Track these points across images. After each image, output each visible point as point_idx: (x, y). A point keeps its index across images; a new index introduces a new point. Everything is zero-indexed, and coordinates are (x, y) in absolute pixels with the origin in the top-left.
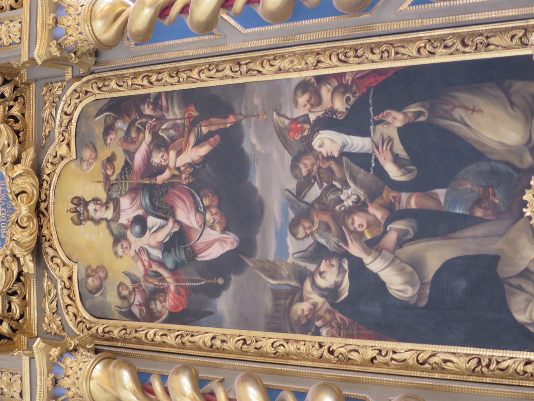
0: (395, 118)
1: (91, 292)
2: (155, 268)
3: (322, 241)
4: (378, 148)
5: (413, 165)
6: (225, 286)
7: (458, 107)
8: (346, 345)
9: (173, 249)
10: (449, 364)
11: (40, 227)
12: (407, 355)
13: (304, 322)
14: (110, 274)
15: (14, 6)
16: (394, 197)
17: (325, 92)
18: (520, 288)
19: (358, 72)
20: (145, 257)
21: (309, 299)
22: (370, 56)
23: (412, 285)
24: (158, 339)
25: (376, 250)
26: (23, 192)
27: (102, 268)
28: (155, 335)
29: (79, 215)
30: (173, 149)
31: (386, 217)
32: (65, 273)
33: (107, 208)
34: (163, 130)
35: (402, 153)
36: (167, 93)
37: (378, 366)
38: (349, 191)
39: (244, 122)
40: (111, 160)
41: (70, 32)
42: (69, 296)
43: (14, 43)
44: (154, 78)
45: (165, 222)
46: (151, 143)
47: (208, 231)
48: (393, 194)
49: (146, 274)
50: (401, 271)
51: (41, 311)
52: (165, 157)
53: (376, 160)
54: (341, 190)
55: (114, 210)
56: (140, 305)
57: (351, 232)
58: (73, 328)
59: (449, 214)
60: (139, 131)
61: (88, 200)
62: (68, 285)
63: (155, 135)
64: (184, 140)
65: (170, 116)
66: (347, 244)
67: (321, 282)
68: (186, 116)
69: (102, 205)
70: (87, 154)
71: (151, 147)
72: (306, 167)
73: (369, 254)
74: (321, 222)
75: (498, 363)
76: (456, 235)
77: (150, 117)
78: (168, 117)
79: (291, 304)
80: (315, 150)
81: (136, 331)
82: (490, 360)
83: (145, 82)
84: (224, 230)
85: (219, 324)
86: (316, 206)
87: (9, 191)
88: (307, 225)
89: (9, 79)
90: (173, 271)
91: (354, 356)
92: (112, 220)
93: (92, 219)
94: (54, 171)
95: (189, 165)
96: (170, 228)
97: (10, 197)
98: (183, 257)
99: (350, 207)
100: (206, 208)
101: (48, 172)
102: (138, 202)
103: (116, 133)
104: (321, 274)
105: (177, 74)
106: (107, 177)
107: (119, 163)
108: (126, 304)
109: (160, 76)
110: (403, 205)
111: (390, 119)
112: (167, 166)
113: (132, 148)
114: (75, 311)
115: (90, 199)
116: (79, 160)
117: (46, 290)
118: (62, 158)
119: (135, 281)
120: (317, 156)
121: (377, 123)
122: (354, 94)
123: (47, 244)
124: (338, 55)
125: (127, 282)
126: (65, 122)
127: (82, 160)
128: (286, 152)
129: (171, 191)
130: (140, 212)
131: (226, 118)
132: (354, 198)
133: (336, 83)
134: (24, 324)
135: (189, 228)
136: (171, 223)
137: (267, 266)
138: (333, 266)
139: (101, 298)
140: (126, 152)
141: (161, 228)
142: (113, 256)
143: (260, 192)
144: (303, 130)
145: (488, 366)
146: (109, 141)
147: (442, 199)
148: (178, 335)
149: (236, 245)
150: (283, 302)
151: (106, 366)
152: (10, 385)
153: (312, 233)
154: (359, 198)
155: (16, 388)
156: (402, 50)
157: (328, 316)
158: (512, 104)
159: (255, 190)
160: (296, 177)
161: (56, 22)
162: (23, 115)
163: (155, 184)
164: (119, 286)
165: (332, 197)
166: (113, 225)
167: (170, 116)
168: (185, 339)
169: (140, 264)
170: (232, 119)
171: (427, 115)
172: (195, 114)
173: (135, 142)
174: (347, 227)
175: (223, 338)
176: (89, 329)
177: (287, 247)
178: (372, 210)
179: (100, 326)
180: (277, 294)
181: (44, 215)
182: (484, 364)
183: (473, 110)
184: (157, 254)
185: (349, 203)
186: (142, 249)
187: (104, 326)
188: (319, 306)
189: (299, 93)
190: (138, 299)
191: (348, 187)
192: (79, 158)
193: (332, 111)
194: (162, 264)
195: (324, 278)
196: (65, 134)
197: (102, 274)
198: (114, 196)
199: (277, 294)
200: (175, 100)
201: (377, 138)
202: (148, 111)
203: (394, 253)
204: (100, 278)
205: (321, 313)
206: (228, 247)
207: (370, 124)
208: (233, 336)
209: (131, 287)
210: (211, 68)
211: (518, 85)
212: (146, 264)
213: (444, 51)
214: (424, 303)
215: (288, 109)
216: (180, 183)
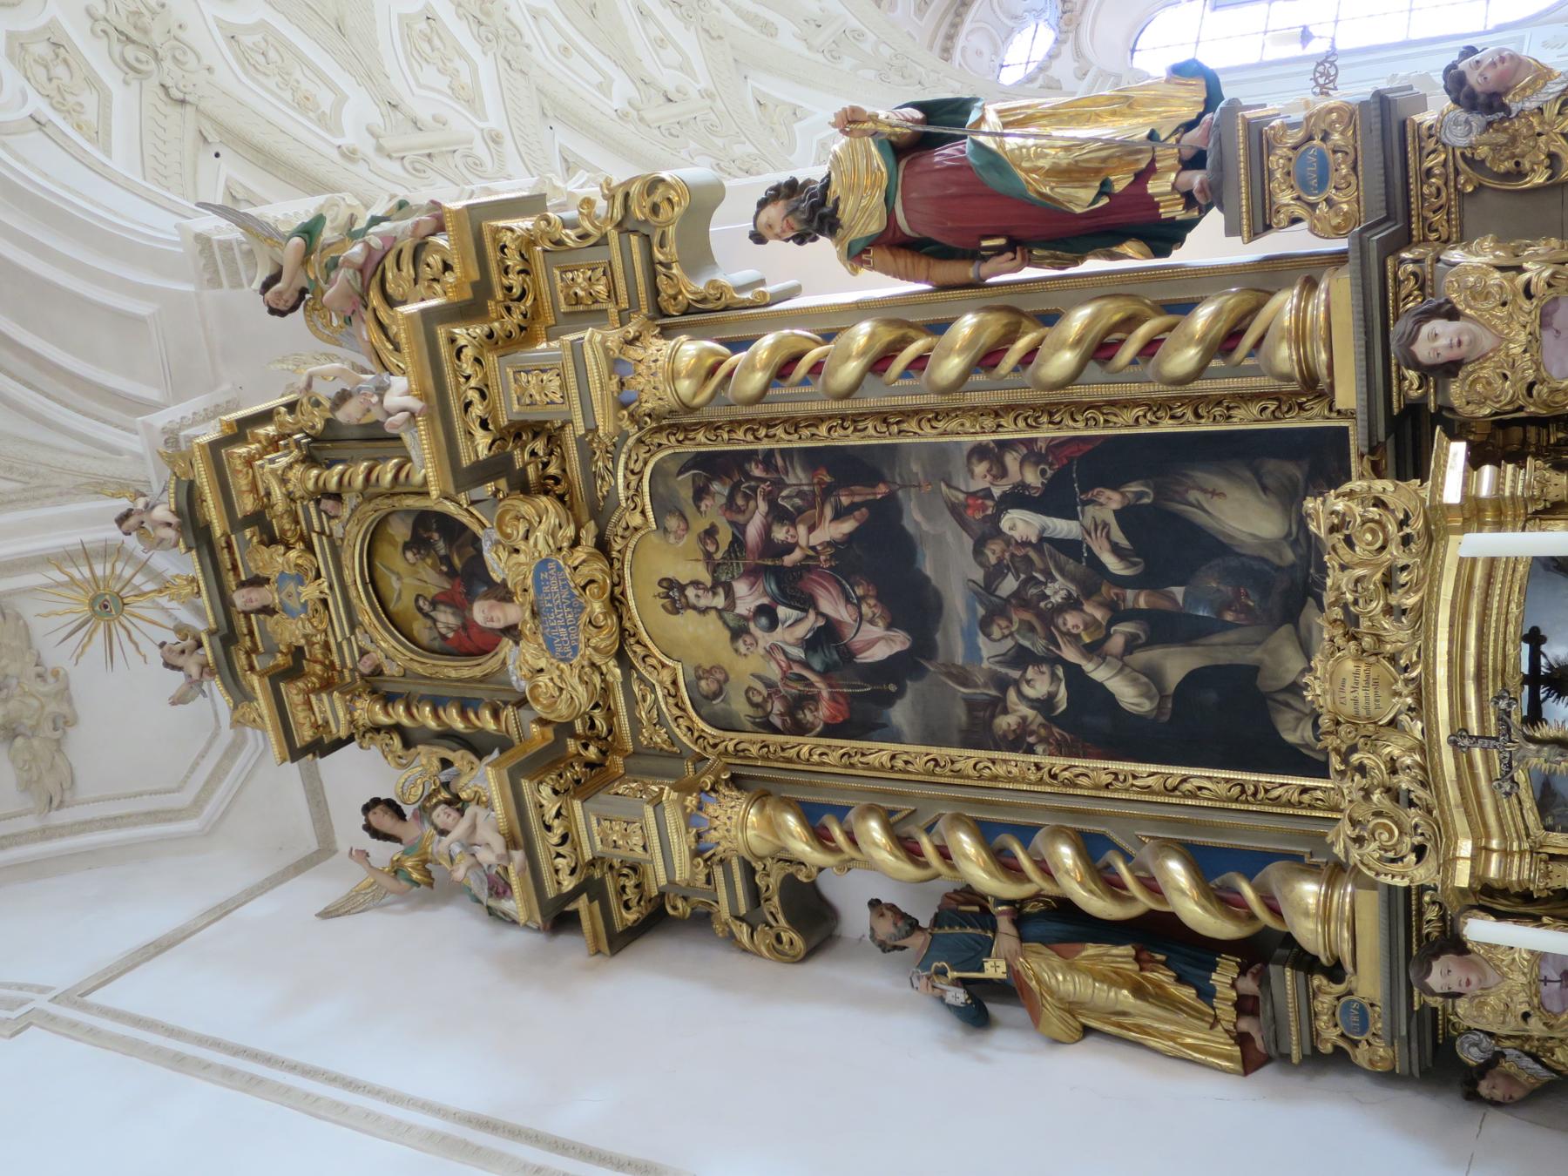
0: (1109, 499)
1: (706, 697)
2: (797, 669)
3: (1027, 644)
4: (1090, 535)
5: (1138, 556)
6: (900, 693)
7: (1193, 488)
8: (1071, 767)
9: (819, 649)
10: (1205, 792)
11: (620, 618)
12: (1151, 781)
13: (1011, 737)
14: (732, 676)
15: (523, 324)
16: (1117, 595)
17: (1011, 460)
18: (1288, 705)
19: (1053, 439)
20: (781, 657)
21: (1015, 711)
22: (1071, 423)
23: (1150, 698)
24: (815, 758)
25: (1099, 656)
26: (592, 581)
27: (720, 668)
28: (810, 755)
29: (674, 601)
30: (802, 522)
31: (1107, 617)
32: (666, 676)
33: (715, 594)
34: (783, 498)
35: (1124, 542)
36: (782, 451)
37: (1116, 790)
38: (1057, 586)
39: (900, 493)
40: (711, 533)
41: (644, 397)
42: (677, 705)
43: (552, 402)
44: (762, 432)
45: (804, 614)
46: (768, 514)
47: (866, 626)
48: (1117, 590)
49: (785, 677)
50: (1134, 682)
51: (635, 722)
52: (792, 531)
53: (1089, 549)
54: (1045, 584)
55: (726, 598)
56: (781, 714)
57: (1063, 634)
58: (691, 746)
59: (1190, 616)
60: (747, 498)
61: (684, 582)
62: (673, 691)
63: (773, 506)
64: (817, 512)
65: (791, 480)
66: (1058, 647)
67: (1029, 691)
68: (816, 480)
69: (706, 589)
70: (673, 523)
71: (770, 519)
72: (994, 553)
73: (1090, 660)
74: (1021, 621)
75: (1267, 791)
76: (1203, 641)
77: (763, 480)
78: (788, 482)
79: (993, 717)
80: (1004, 534)
81: (783, 750)
82: (1256, 787)
83: (750, 437)
84: (889, 627)
85: (896, 738)
86: (1013, 601)
87: (572, 585)
88: (1004, 623)
89: (538, 429)
90: (824, 674)
91: (1083, 781)
92: (724, 609)
93: (694, 608)
94: (626, 546)
95: (829, 544)
96: (811, 622)
97: (576, 593)
98: (836, 657)
99: (1059, 604)
100: (860, 599)
101: (617, 547)
102: (760, 587)
103: (713, 498)
104: (1028, 682)
105: (796, 431)
106: (708, 556)
107: (725, 536)
108: (760, 713)
109: (772, 431)
110: (1130, 604)
111: (1102, 500)
112: (796, 545)
113: (740, 518)
114: (688, 723)
115: (687, 582)
116: (661, 531)
117: (639, 697)
118: (636, 529)
119: (769, 685)
120: (1008, 541)
121: (1085, 503)
122: (1051, 465)
123: (632, 640)
124: (1026, 419)
125: (759, 686)
126: (633, 484)
127: (666, 530)
128: (965, 534)
129: (806, 575)
130: (765, 601)
131: (874, 486)
132: (1063, 593)
133: (1025, 451)
134: (614, 740)
135: (840, 622)
136: (812, 615)
137: (954, 671)
138: (1043, 673)
139: (722, 705)
140: (733, 523)
141: (797, 621)
142: (733, 653)
143: (934, 582)
144: (985, 508)
145: (1255, 794)
146: (703, 508)
147: (1180, 599)
148: (843, 755)
149: (907, 645)
150: (982, 714)
151: (761, 809)
152: (626, 835)
153: (1011, 634)
154: (1070, 594)
155: (636, 840)
156: (1113, 419)
157: (1043, 732)
158: (1265, 489)
159: (927, 579)
160: (981, 565)
161: (622, 384)
162: (564, 470)
163: (782, 567)
164: (747, 692)
165: (1033, 591)
166: (728, 616)
167: (791, 480)
168: (855, 760)
169: (774, 665)
170: (882, 490)
171: (1152, 496)
172: (828, 479)
173: (744, 512)
174: (1057, 628)
175: (905, 757)
176: (715, 746)
177: (980, 649)
178: (1088, 608)
179: (731, 740)
180: (972, 705)
181: (621, 603)
182: (1249, 792)
183: (1214, 493)
184: (798, 653)
185: (1057, 599)
186: (774, 647)
187: (735, 741)
188: (1030, 719)
189: (974, 460)
190: (778, 707)
191: (1054, 580)
192: (662, 529)
193: (1023, 485)
194: (806, 665)
195: (1033, 687)
196: (636, 499)
197: (720, 677)
198: (723, 578)
199: (972, 705)
200: (796, 459)
201: (1088, 522)
202: (757, 472)
203: (1121, 660)
204: (718, 681)
205: (1034, 727)
206: (897, 648)
207: (1076, 505)
208: (918, 755)
209: (765, 693)
210: (846, 424)
211: (1271, 465)
212: (783, 664)
213: (1171, 422)
214: (1166, 718)
215: (961, 480)
216: (818, 566)
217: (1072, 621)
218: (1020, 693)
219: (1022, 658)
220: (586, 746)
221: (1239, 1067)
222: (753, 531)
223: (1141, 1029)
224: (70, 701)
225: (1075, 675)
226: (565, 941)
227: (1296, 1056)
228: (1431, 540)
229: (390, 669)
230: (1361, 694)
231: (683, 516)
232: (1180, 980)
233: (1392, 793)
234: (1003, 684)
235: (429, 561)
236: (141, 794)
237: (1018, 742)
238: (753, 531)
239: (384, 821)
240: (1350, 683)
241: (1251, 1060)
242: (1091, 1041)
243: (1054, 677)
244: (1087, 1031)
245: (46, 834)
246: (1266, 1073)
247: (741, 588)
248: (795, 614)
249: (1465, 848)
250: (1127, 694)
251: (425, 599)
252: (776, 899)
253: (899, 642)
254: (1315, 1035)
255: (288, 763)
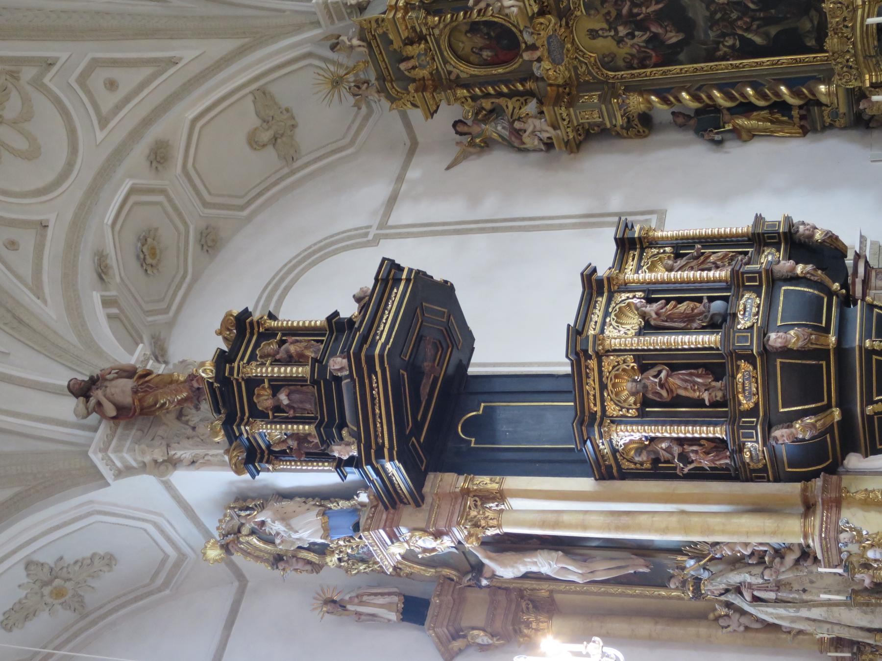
3: (725, 31)
6: (682, 50)
40: (609, 13)
42: (597, 68)
46: (630, 6)
54: (730, 14)
57: (737, 27)
67: (727, 44)
70: (592, 12)
81: (640, 75)
93: (602, 36)
100: (666, 26)
107: (614, 13)
112: (642, 13)
130: (630, 31)
132: (737, 16)
140: (617, 10)
141: (642, 36)
157: (732, 54)
190: (636, 61)
191: (733, 12)
192: (588, 14)
197: (613, 56)
217: (740, 23)
218: (724, 45)
219: (724, 35)
220: (565, 89)
221: (802, 135)
222: (625, 11)
223: (772, 132)
224: (294, 118)
225: (742, 38)
226: (553, 153)
227: (819, 128)
228: (854, 11)
229: (463, 75)
230: (839, 46)
231: (596, 9)
232: (783, 116)
233: (847, 66)
234: (718, 43)
235: (479, 35)
236: (328, 145)
237: (724, 58)
238: (625, 11)
239: (460, 128)
240: (836, 45)
241: (805, 132)
242: (755, 138)
243: (735, 39)
244: (754, 135)
245: (293, 172)
246: (809, 135)
247: (620, 28)
248: (641, 33)
249: (867, 77)
250: (758, 40)
251: (476, 48)
252: (637, 120)
253: (681, 36)
254: (824, 122)
255: (429, 120)
